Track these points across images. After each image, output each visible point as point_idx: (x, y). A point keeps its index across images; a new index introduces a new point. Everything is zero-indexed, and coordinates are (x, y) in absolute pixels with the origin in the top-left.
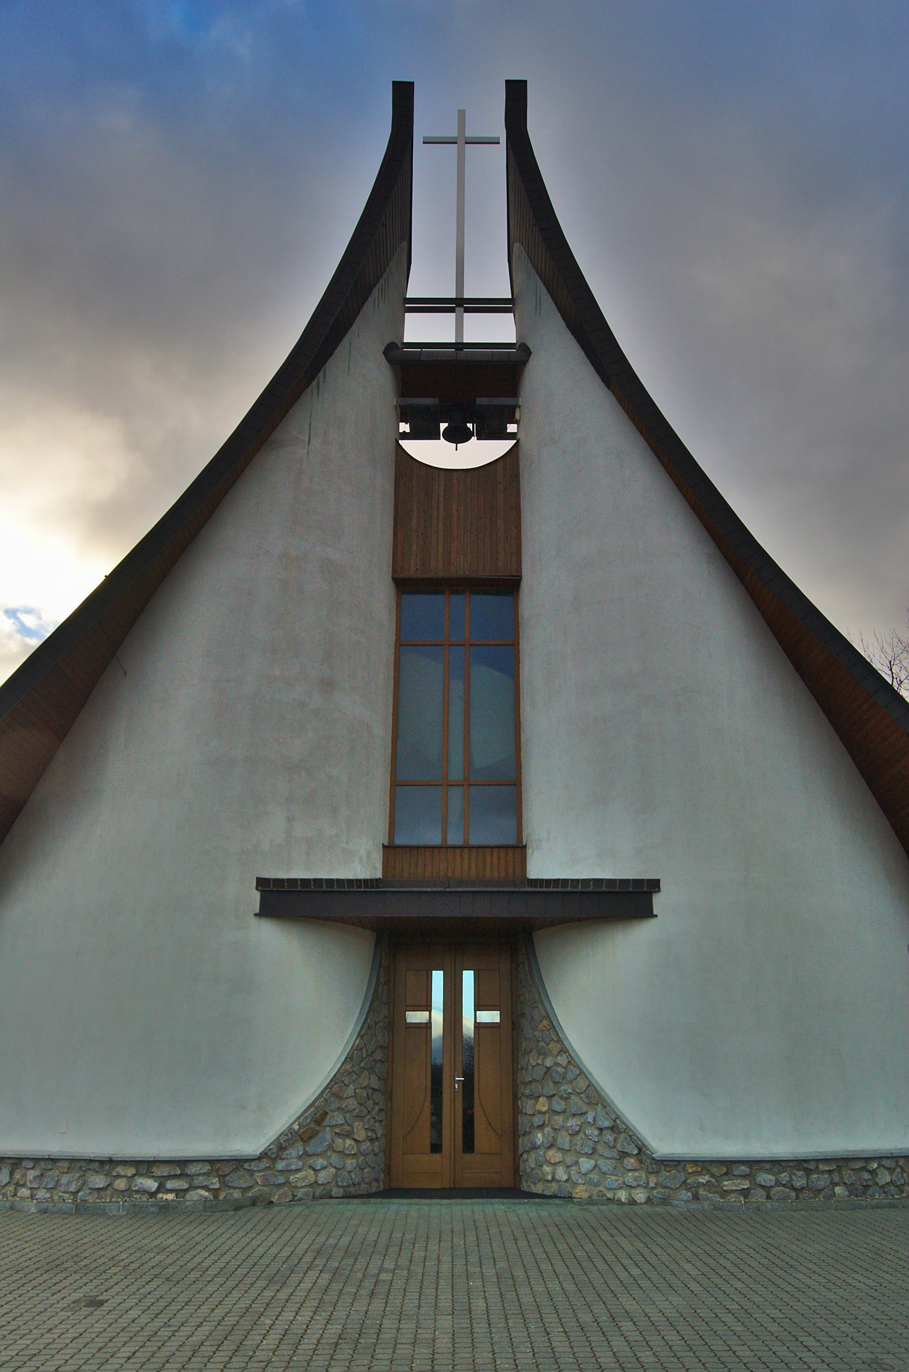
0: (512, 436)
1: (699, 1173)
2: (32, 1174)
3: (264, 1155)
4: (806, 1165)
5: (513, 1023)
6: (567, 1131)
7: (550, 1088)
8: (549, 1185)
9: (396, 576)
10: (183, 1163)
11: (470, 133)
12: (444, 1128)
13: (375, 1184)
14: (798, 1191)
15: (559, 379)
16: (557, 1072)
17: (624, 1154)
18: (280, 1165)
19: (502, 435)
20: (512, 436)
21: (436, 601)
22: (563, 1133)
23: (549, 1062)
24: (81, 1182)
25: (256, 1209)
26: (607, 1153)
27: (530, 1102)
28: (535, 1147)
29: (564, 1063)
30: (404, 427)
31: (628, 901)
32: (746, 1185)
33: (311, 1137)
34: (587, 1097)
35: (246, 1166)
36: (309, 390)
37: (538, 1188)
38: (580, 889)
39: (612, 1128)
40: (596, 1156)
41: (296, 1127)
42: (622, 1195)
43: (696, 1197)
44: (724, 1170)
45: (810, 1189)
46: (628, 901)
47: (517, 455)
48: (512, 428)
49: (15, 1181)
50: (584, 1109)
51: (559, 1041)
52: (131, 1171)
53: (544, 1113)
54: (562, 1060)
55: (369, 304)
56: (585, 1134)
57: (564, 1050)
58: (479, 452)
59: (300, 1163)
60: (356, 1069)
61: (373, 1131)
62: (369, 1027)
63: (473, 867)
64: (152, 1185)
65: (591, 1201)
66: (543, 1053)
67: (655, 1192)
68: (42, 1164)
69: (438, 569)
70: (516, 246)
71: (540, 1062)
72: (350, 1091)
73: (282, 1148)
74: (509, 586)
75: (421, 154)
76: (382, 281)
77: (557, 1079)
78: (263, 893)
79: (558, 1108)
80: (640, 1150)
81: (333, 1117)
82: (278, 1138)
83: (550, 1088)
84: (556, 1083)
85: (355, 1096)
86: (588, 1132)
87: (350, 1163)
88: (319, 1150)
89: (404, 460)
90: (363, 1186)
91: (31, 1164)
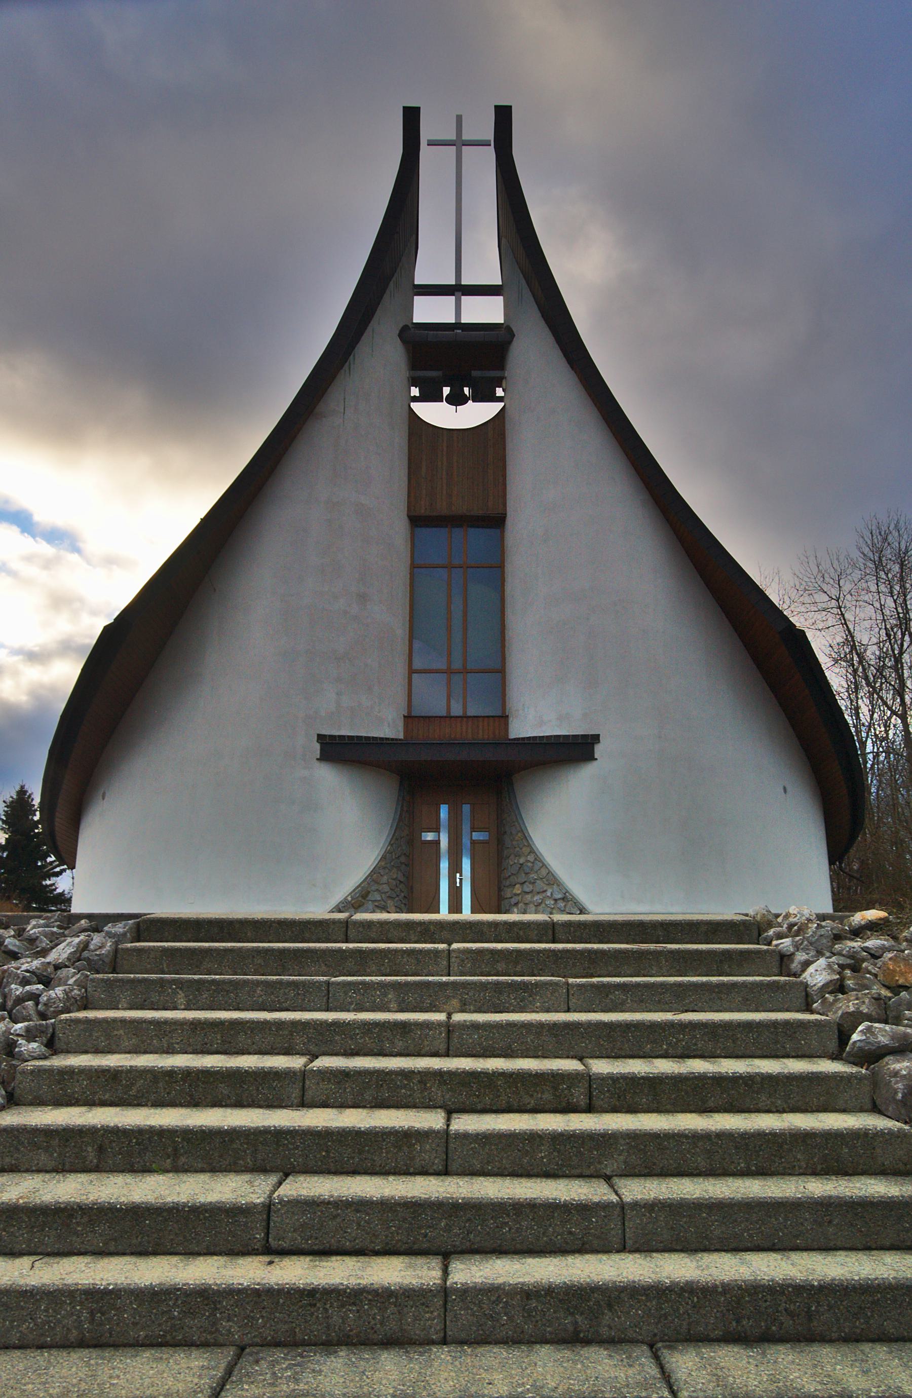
0: (500, 399)
5: (498, 840)
11: (465, 137)
15: (533, 354)
19: (491, 398)
21: (441, 534)
22: (532, 905)
23: (522, 861)
30: (415, 392)
31: (577, 750)
33: (360, 906)
36: (342, 371)
39: (563, 899)
41: (349, 899)
46: (577, 750)
47: (504, 418)
51: (529, 846)
53: (518, 895)
54: (531, 858)
55: (386, 297)
57: (532, 851)
58: (475, 414)
60: (388, 865)
62: (397, 839)
63: (470, 730)
66: (518, 855)
69: (442, 508)
70: (503, 240)
74: (496, 522)
75: (426, 153)
76: (396, 274)
77: (528, 870)
78: (321, 744)
79: (527, 890)
82: (338, 905)
83: (522, 877)
84: (526, 874)
85: (388, 883)
86: (548, 903)
89: (414, 418)
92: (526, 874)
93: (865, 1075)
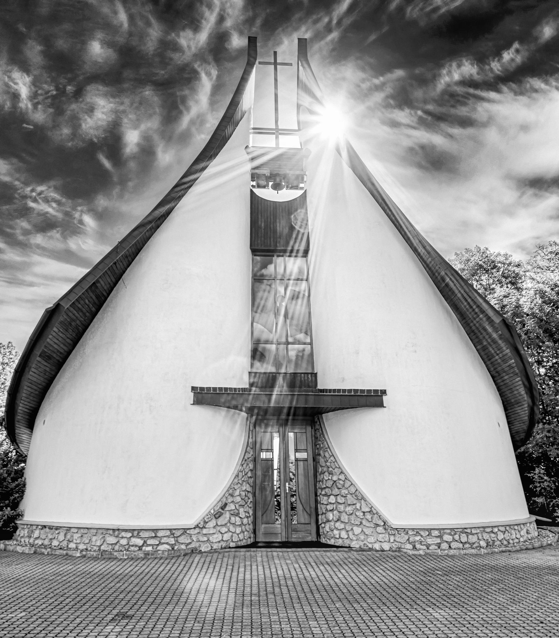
0: (302, 188)
1: (415, 535)
2: (76, 536)
3: (197, 526)
4: (466, 531)
6: (346, 513)
7: (336, 491)
8: (337, 540)
9: (253, 248)
10: (155, 531)
12: (286, 512)
13: (249, 540)
14: (464, 544)
16: (340, 484)
17: (377, 525)
18: (205, 531)
20: (302, 188)
22: (344, 514)
23: (335, 478)
24: (103, 540)
25: (194, 555)
26: (368, 524)
27: (325, 498)
28: (328, 521)
29: (343, 478)
32: (438, 541)
33: (219, 516)
34: (356, 496)
35: (188, 532)
37: (332, 542)
38: (353, 393)
40: (362, 526)
42: (377, 546)
43: (414, 547)
44: (427, 533)
45: (469, 543)
48: (302, 185)
49: (66, 539)
50: (354, 503)
52: (129, 535)
53: (333, 504)
54: (342, 477)
56: (356, 515)
59: (215, 530)
61: (248, 513)
62: (246, 460)
64: (140, 542)
65: (361, 550)
67: (393, 544)
68: (82, 530)
71: (330, 478)
72: (237, 493)
73: (206, 523)
77: (340, 486)
79: (339, 501)
80: (385, 523)
81: (230, 506)
85: (240, 495)
86: (358, 514)
87: (238, 530)
88: (223, 523)
90: (244, 541)
91: (76, 530)
92: (339, 489)
93: (56, 94)
